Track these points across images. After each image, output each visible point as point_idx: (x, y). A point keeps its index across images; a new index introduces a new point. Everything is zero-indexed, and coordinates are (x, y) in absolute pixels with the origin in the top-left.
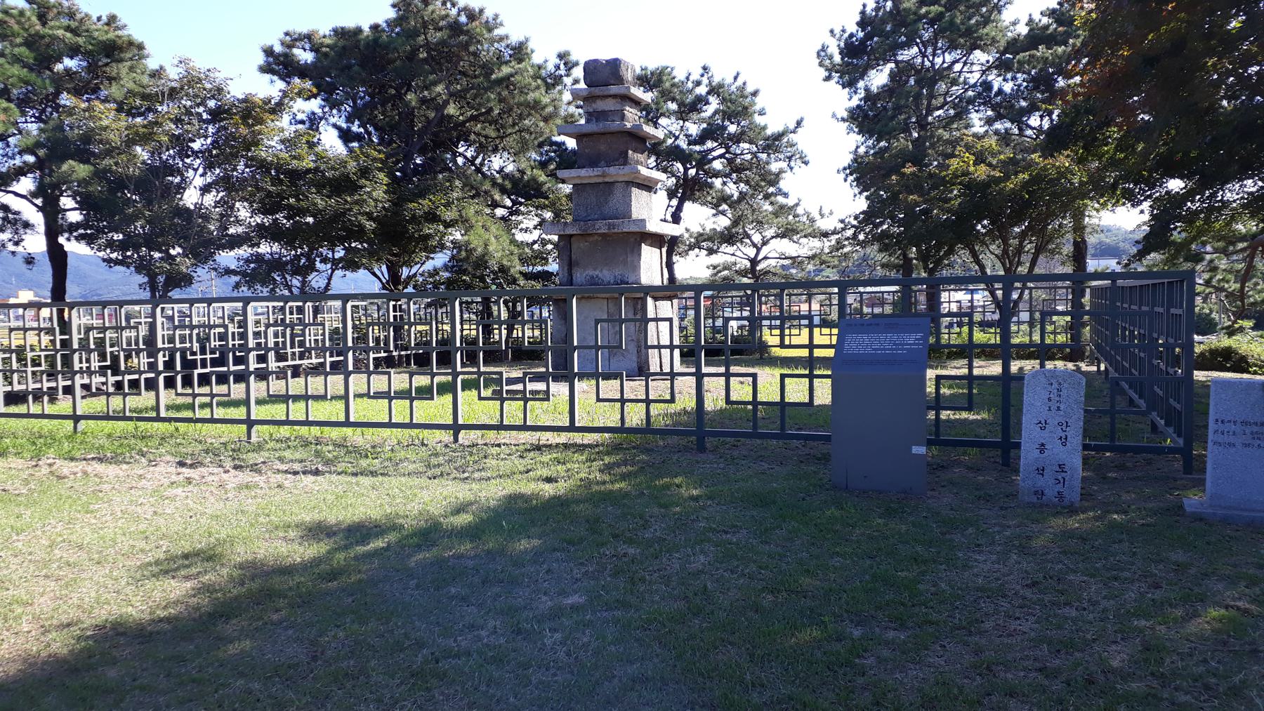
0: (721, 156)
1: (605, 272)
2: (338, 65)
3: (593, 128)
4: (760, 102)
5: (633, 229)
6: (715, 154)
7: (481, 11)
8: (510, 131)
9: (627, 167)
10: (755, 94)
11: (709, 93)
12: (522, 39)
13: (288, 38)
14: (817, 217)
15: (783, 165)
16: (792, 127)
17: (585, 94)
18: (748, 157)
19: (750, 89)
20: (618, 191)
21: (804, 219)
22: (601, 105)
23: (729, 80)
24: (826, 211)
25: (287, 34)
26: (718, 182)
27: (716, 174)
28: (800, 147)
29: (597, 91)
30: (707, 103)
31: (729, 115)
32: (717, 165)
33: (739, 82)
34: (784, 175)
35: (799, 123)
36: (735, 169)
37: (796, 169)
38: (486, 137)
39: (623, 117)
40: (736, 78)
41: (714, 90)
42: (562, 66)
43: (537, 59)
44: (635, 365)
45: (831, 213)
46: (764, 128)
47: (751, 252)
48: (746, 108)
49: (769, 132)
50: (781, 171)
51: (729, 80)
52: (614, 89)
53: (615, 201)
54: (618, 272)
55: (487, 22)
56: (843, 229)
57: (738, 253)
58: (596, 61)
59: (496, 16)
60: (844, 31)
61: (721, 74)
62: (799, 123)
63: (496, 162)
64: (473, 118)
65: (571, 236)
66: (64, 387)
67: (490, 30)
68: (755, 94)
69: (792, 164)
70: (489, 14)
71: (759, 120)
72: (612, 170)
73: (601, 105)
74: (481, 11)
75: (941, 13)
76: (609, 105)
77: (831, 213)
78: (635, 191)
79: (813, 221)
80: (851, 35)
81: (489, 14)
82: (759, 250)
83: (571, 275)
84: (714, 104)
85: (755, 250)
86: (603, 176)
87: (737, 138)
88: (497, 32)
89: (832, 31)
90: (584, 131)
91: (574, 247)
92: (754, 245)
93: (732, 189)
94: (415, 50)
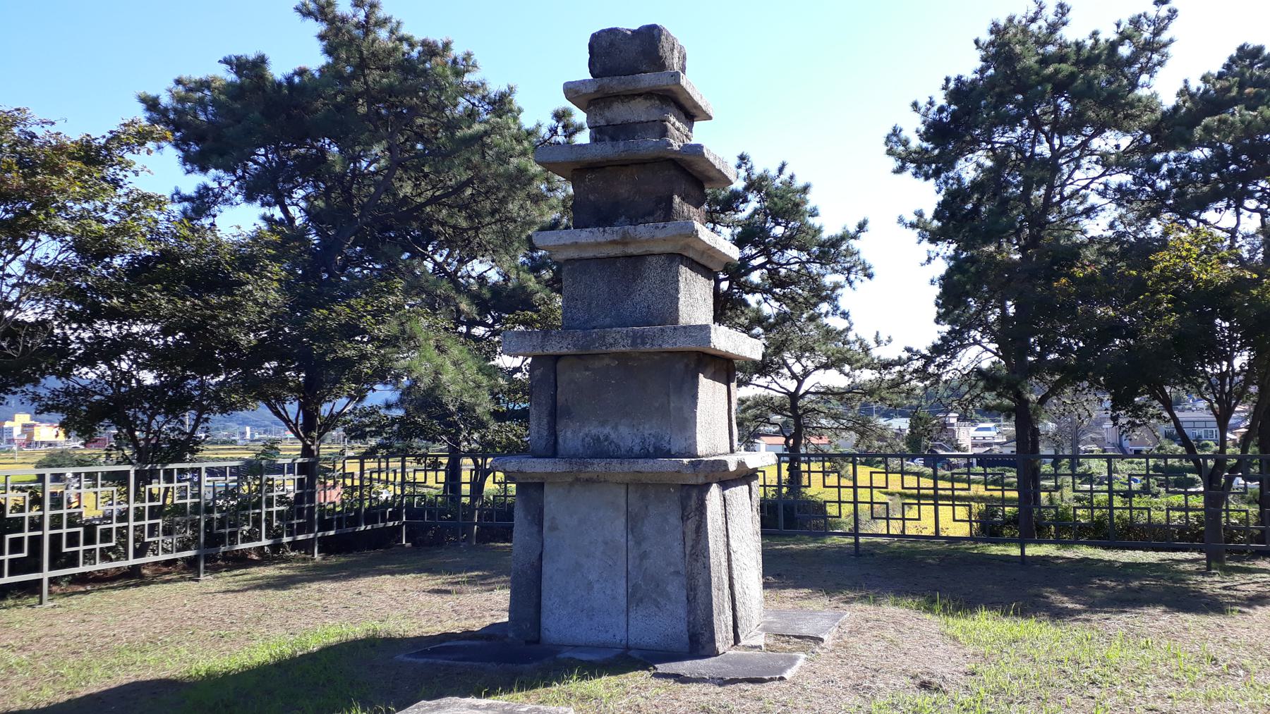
0: (761, 266)
1: (624, 430)
2: (232, 121)
3: (608, 150)
4: (812, 200)
5: (683, 344)
6: (755, 262)
7: (447, 46)
8: (488, 219)
9: (670, 225)
10: (805, 189)
11: (747, 189)
12: (504, 88)
13: (180, 88)
14: (872, 344)
15: (840, 278)
16: (852, 229)
17: (591, 89)
18: (796, 267)
19: (799, 183)
20: (653, 273)
21: (856, 347)
22: (622, 112)
23: (773, 172)
24: (883, 337)
25: (178, 82)
26: (752, 299)
27: (754, 289)
28: (862, 256)
29: (615, 84)
30: (745, 201)
31: (777, 214)
32: (755, 277)
33: (785, 176)
34: (839, 291)
35: (862, 227)
36: (776, 283)
37: (857, 283)
38: (454, 227)
39: (664, 132)
40: (781, 170)
41: (755, 184)
42: (560, 130)
43: (527, 122)
44: (682, 627)
45: (890, 340)
46: (819, 231)
47: (792, 386)
48: (797, 205)
49: (825, 235)
50: (837, 286)
51: (773, 172)
52: (648, 80)
53: (645, 292)
54: (649, 429)
55: (455, 61)
56: (910, 359)
57: (774, 386)
58: (613, 32)
59: (468, 56)
60: (931, 103)
61: (763, 164)
62: (862, 227)
63: (477, 267)
64: (433, 200)
65: (557, 358)
66: (32, 519)
67: (459, 74)
68: (805, 189)
69: (852, 277)
70: (457, 51)
71: (811, 221)
72: (643, 230)
73: (622, 112)
74: (447, 46)
75: (1072, 73)
76: (638, 111)
77: (890, 340)
78: (685, 273)
79: (866, 350)
80: (941, 110)
81: (457, 51)
82: (800, 383)
83: (553, 433)
84: (753, 203)
85: (795, 383)
86: (624, 242)
87: (784, 244)
88: (468, 77)
89: (915, 105)
90: (588, 157)
91: (562, 379)
92: (794, 376)
93: (770, 308)
94: (353, 99)
